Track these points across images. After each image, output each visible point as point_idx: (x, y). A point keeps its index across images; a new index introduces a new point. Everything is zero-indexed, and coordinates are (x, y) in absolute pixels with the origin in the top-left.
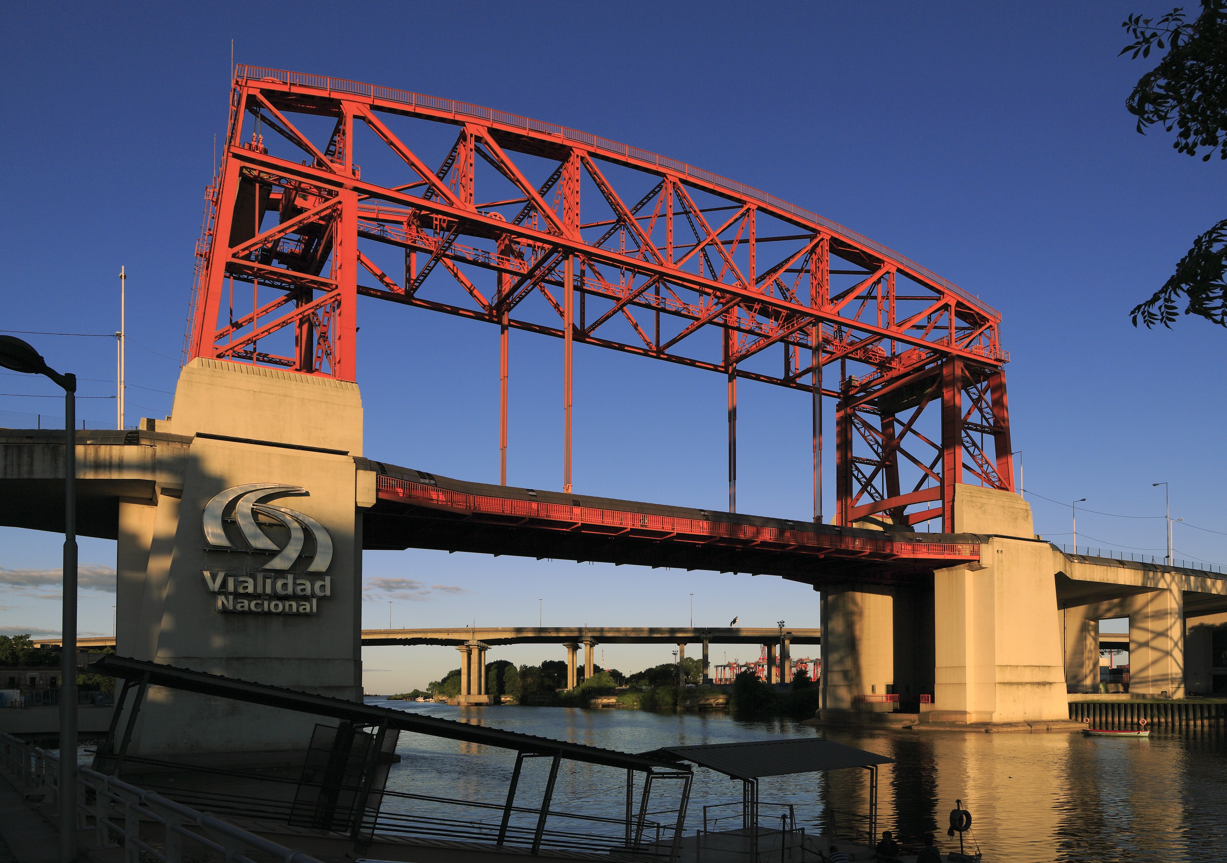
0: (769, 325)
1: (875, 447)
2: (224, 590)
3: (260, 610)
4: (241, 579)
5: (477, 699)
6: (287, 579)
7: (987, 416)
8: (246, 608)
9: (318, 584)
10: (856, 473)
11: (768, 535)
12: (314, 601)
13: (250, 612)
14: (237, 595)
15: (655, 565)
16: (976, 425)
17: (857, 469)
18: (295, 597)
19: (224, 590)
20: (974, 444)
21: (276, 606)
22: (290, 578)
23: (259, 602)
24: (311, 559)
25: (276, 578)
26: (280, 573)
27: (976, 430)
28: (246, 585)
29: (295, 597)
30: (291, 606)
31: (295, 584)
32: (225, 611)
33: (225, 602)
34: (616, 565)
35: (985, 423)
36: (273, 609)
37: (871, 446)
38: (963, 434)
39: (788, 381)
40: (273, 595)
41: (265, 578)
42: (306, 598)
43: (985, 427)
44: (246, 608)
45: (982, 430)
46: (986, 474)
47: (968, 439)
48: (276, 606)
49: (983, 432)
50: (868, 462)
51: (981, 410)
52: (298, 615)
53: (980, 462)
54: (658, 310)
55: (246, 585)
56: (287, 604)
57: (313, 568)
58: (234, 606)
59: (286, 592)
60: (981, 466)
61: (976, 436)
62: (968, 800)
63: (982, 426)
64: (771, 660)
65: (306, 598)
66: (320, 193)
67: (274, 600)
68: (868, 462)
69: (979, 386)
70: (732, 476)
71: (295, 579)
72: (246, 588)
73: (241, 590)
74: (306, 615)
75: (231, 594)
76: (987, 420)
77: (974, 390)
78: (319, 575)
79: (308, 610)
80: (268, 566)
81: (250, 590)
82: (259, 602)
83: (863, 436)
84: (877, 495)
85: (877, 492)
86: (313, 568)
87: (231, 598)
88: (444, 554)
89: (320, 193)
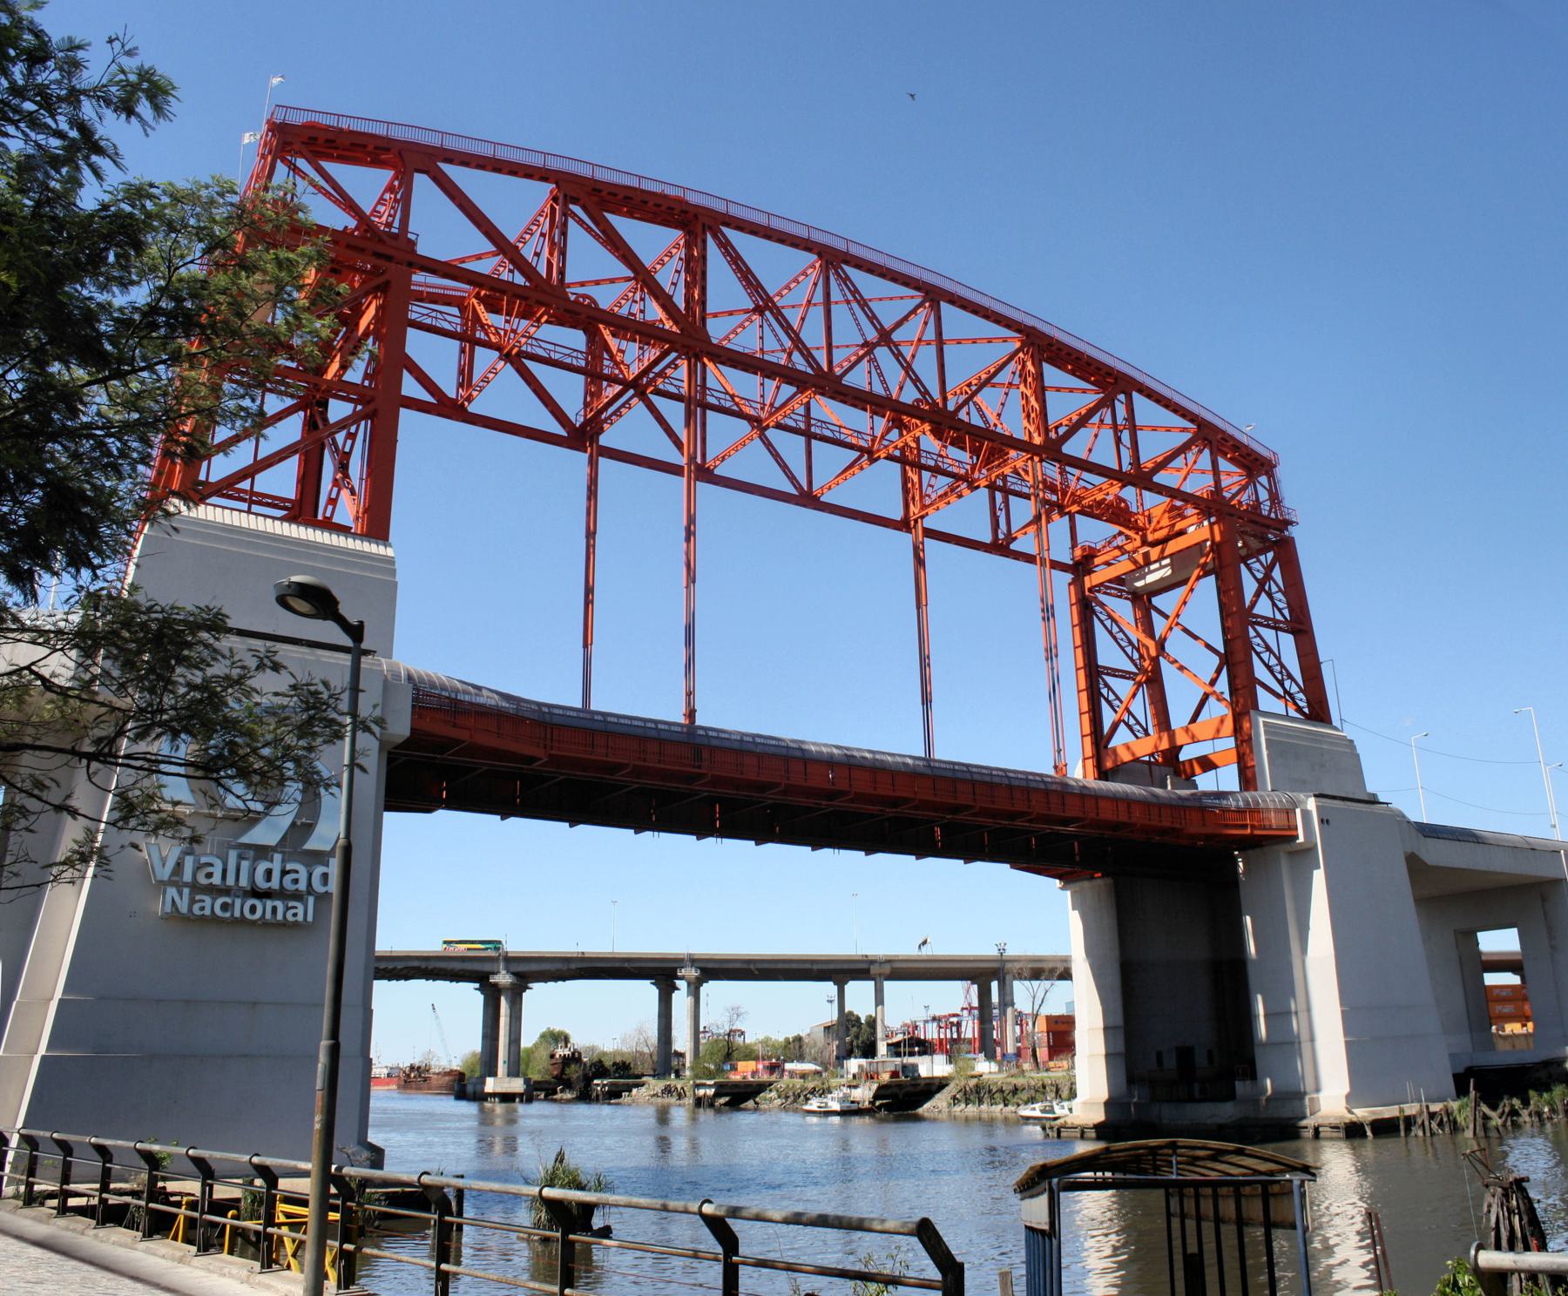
0: (959, 458)
1: (1129, 649)
2: (176, 878)
3: (228, 915)
4: (204, 860)
5: (506, 1085)
6: (272, 861)
7: (1281, 605)
8: (207, 912)
9: (318, 871)
10: (1104, 691)
11: (494, 701)
12: (311, 900)
13: (214, 919)
14: (196, 888)
15: (816, 845)
16: (1267, 619)
17: (1106, 685)
18: (282, 894)
19: (176, 878)
20: (1268, 648)
21: (253, 909)
22: (278, 857)
23: (228, 900)
24: (308, 829)
25: (256, 859)
26: (262, 852)
27: (1268, 626)
28: (210, 869)
29: (282, 894)
30: (274, 909)
31: (284, 873)
32: (175, 916)
33: (177, 899)
34: (757, 844)
35: (1278, 617)
36: (290, 917)
37: (1123, 649)
38: (1252, 633)
39: (1000, 547)
40: (249, 888)
41: (241, 857)
42: (298, 896)
43: (1280, 622)
44: (207, 912)
45: (1275, 626)
46: (1291, 695)
47: (1258, 640)
48: (253, 909)
49: (1277, 629)
50: (1125, 675)
51: (1270, 595)
52: (284, 924)
53: (1279, 676)
54: (809, 436)
55: (210, 869)
56: (269, 904)
57: (311, 845)
58: (190, 909)
59: (269, 885)
60: (1281, 683)
61: (1268, 634)
62: (1367, 1278)
63: (1274, 620)
64: (984, 1011)
65: (298, 896)
66: (597, 347)
67: (221, 896)
68: (1125, 675)
69: (1262, 558)
70: (926, 699)
71: (283, 861)
72: (209, 875)
73: (202, 880)
74: (296, 925)
75: (186, 885)
76: (1280, 610)
77: (1257, 566)
78: (319, 857)
79: (300, 918)
80: (245, 839)
81: (216, 880)
82: (228, 900)
83: (1110, 632)
84: (1138, 727)
85: (1138, 723)
86: (311, 845)
87: (186, 891)
88: (626, 834)
89: (597, 347)
